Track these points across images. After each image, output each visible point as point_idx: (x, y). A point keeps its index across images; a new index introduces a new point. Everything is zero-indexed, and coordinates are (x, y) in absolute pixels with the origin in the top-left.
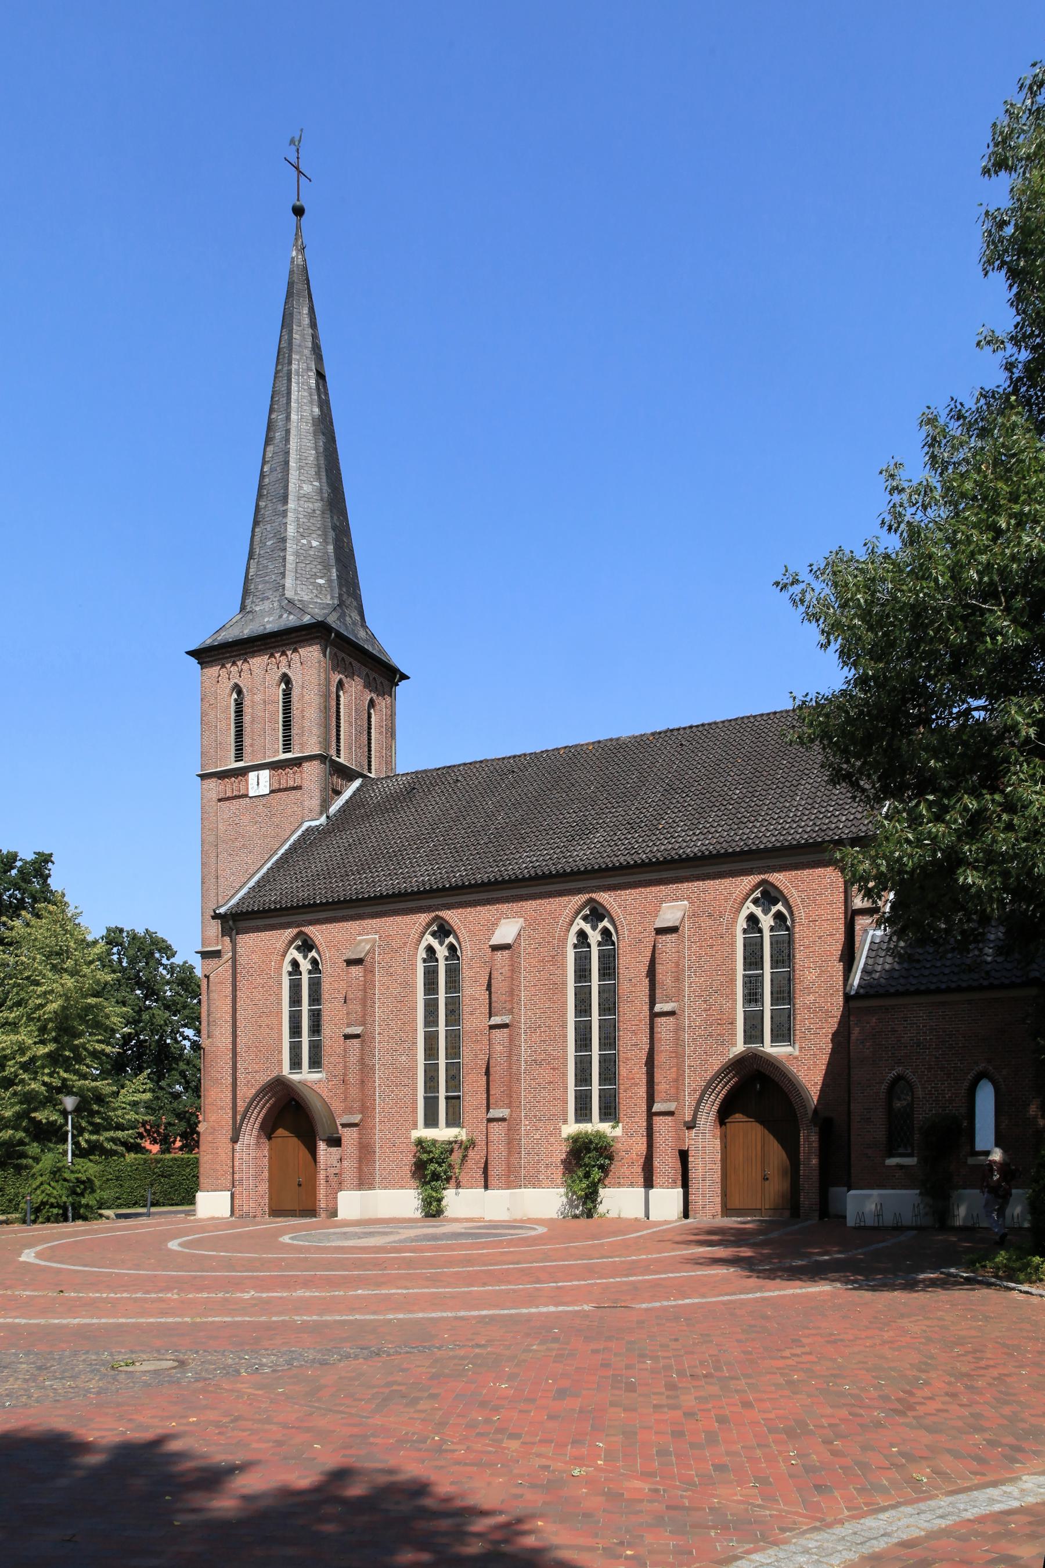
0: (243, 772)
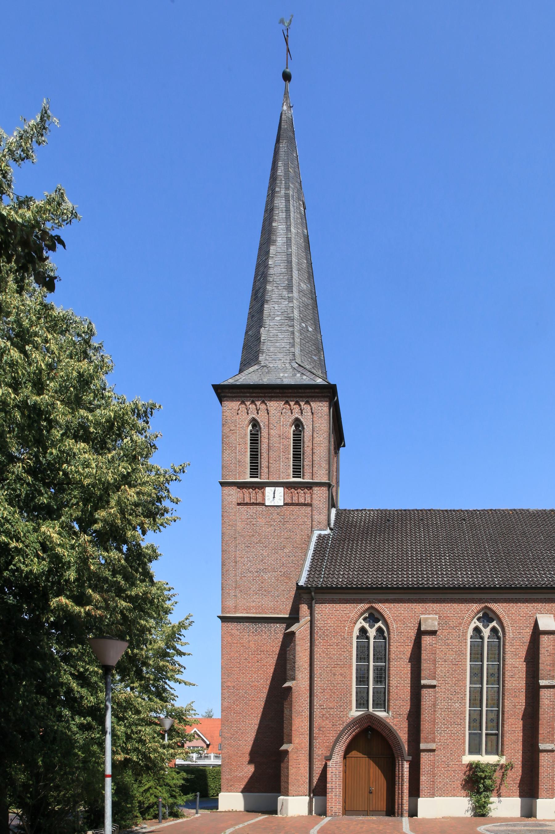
0: (262, 486)
